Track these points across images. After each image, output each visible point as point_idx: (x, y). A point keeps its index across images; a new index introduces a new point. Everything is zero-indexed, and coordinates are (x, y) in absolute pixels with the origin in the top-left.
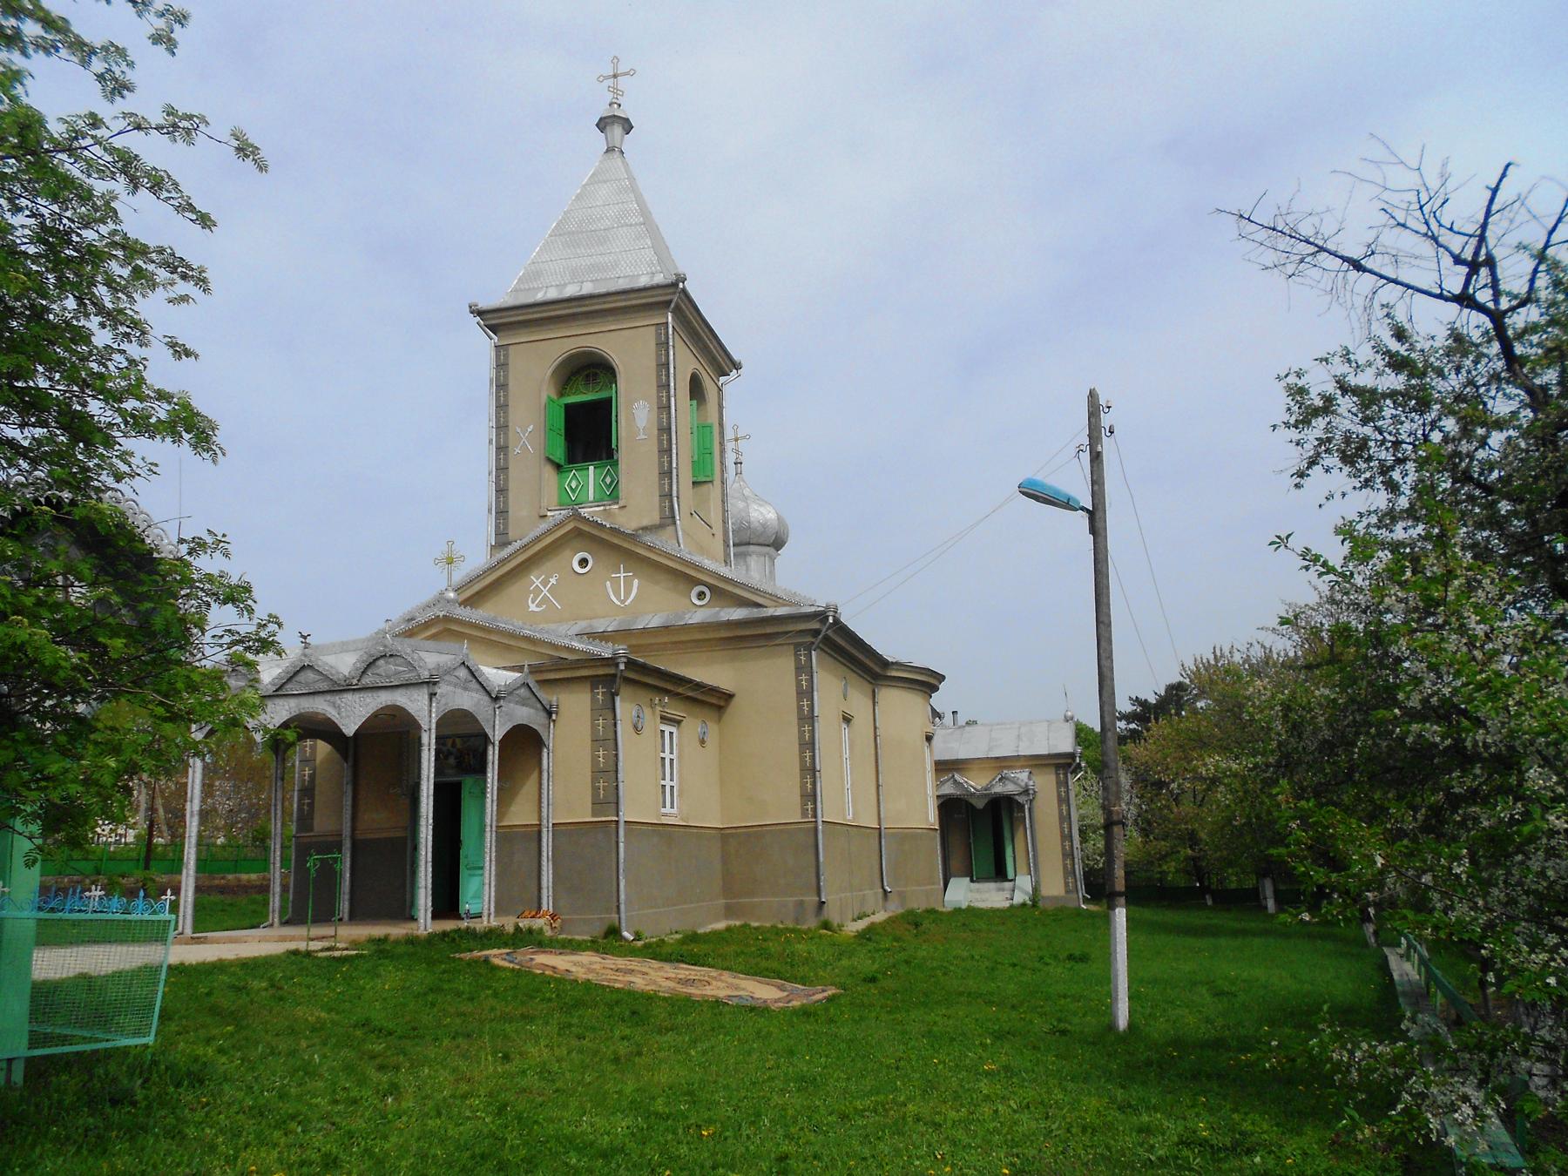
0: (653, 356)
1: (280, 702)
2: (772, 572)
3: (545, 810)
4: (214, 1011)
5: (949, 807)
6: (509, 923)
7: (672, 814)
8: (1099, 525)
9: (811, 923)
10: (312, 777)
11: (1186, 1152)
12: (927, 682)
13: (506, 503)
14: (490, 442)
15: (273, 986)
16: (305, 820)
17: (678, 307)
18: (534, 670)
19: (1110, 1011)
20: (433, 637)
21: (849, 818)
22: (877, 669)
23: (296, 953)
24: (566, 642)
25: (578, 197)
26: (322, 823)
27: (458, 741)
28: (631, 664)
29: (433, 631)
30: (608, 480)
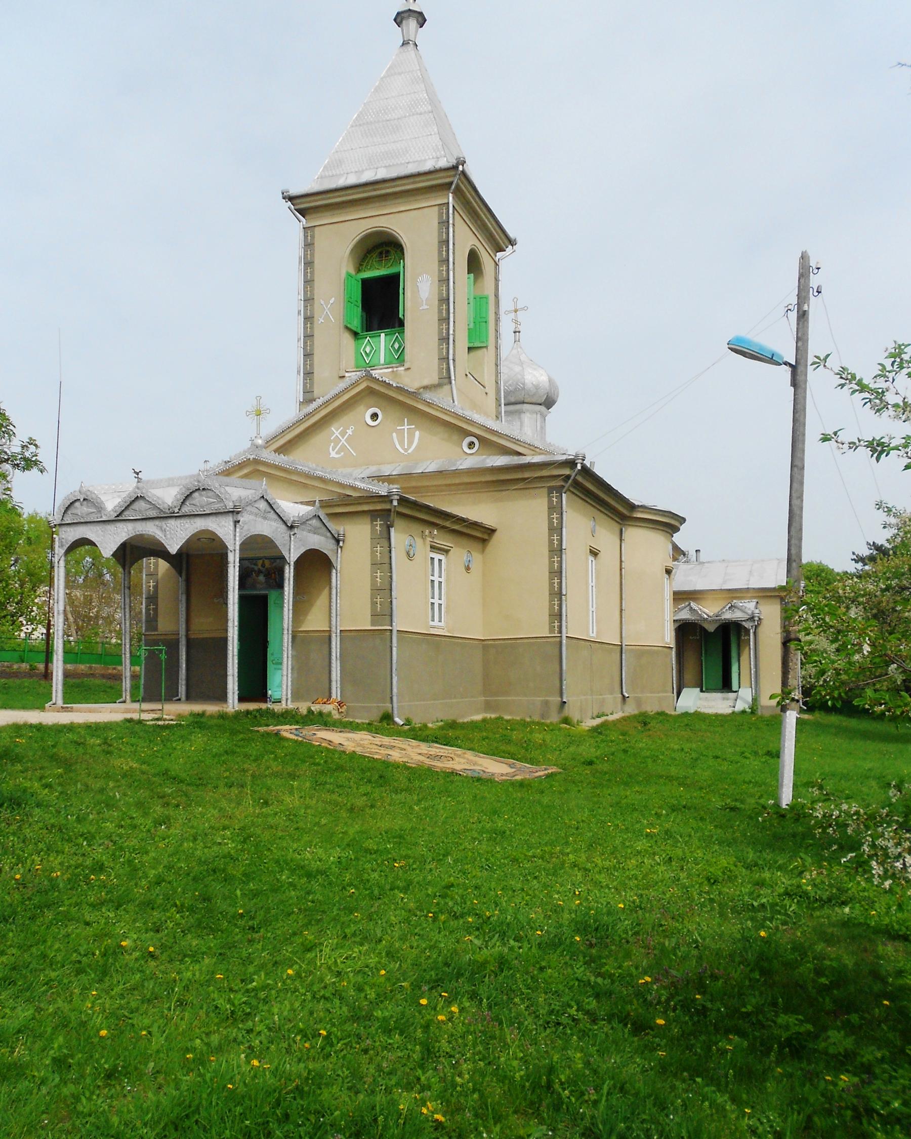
0: (436, 234)
1: (120, 525)
2: (543, 428)
3: (334, 619)
4: (54, 758)
5: (686, 632)
6: (303, 708)
7: (440, 626)
8: (800, 378)
9: (554, 718)
10: (156, 587)
11: (787, 902)
12: (669, 524)
13: (312, 365)
14: (299, 312)
15: (105, 743)
16: (152, 622)
17: (458, 188)
18: (324, 504)
19: (776, 795)
20: (246, 476)
21: (592, 635)
22: (625, 512)
23: (130, 721)
24: (351, 482)
25: (377, 90)
26: (164, 625)
27: (267, 563)
28: (403, 501)
29: (245, 471)
30: (396, 346)
